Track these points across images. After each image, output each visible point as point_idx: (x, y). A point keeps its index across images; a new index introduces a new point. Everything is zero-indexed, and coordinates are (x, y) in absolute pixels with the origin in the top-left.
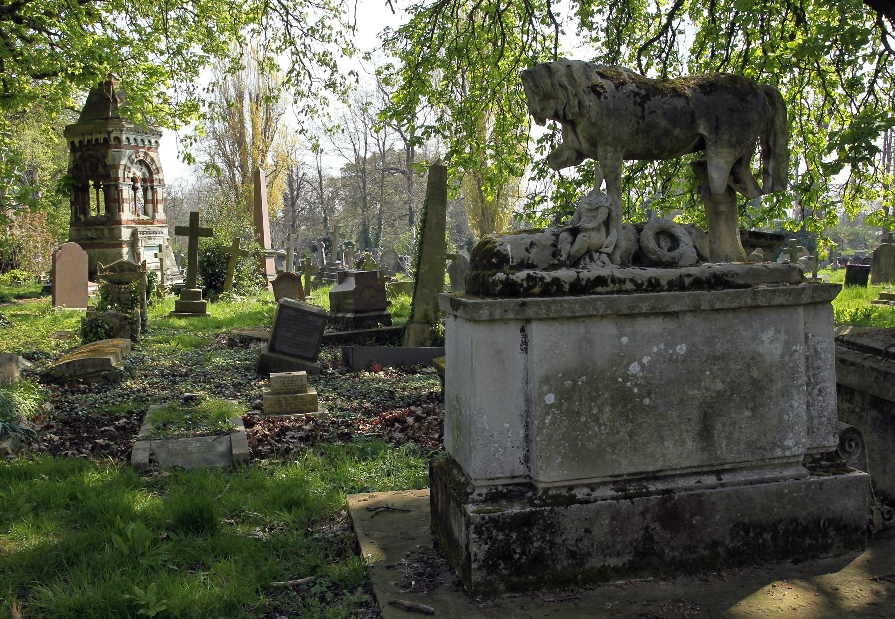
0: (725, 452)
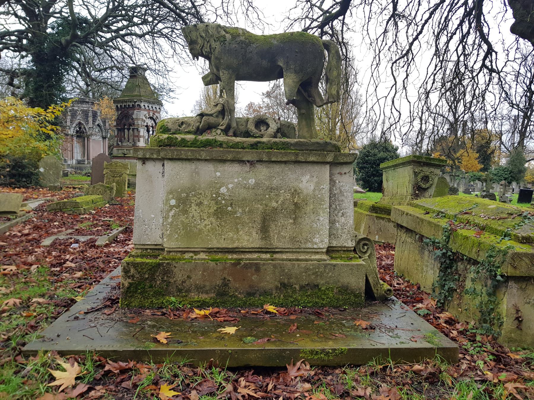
0: (276, 243)
